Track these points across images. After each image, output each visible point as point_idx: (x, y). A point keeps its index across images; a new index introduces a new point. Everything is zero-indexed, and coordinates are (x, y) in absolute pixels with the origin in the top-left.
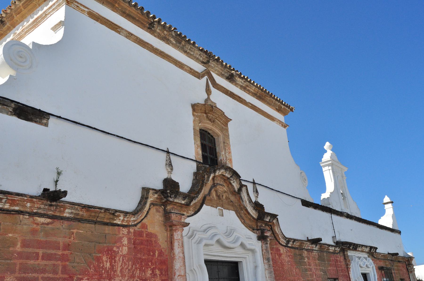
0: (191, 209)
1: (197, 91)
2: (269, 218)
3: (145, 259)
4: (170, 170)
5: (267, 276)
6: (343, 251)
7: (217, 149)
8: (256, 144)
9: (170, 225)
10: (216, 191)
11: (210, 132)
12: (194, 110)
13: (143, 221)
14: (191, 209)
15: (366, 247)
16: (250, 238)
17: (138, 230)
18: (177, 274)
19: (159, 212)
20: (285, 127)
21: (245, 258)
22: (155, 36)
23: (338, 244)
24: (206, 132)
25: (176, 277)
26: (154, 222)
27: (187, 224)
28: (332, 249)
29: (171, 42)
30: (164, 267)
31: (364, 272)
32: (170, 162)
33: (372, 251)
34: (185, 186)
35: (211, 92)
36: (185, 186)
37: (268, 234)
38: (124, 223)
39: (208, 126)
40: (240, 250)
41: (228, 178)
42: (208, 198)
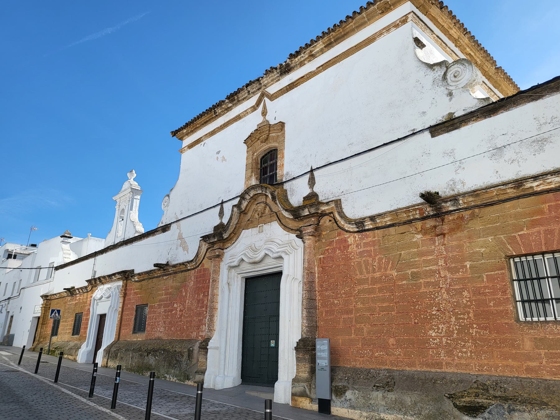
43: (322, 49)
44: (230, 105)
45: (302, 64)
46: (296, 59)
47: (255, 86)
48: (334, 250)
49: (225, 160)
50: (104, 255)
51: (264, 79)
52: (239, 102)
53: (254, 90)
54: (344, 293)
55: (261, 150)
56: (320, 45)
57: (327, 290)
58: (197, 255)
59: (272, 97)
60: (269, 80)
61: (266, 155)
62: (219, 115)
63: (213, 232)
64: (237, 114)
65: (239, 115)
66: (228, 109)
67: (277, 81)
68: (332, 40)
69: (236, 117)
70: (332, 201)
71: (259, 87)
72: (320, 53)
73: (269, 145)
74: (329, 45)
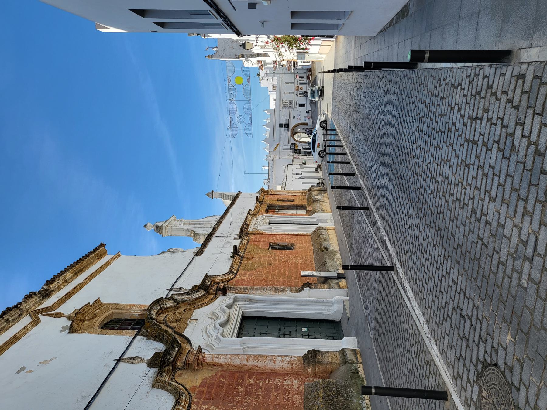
0: (184, 345)
2: (207, 281)
4: (140, 360)
6: (247, 234)
7: (126, 317)
8: (133, 280)
9: (197, 363)
10: (171, 322)
11: (106, 322)
12: (76, 331)
14: (184, 345)
15: (247, 216)
16: (222, 301)
18: (245, 362)
19: (181, 374)
20: (119, 255)
21: (240, 308)
23: (240, 236)
25: (247, 364)
26: (190, 380)
27: (200, 348)
28: (245, 242)
30: (237, 374)
31: (268, 223)
32: (130, 358)
33: (252, 214)
34: (160, 347)
35: (60, 313)
36: (160, 347)
37: (222, 285)
38: (186, 407)
39: (99, 321)
40: (232, 311)
41: (161, 309)
42: (176, 330)
45: (59, 288)
46: (53, 285)
49: (207, 195)
50: (234, 206)
56: (69, 275)
69: (12, 339)
73: (102, 317)
74: (76, 274)
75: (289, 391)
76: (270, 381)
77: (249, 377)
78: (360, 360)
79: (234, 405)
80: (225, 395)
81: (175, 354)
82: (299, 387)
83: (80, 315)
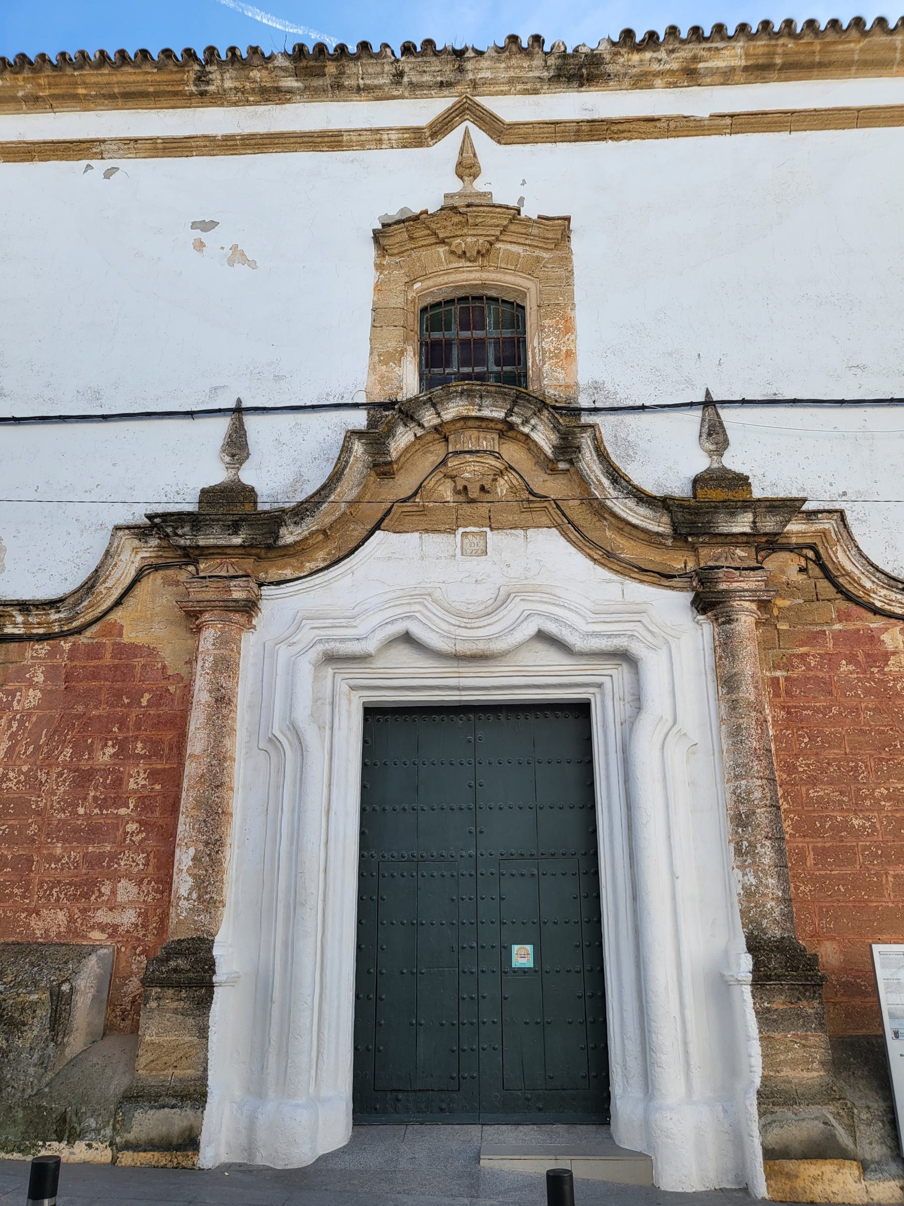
1: (479, 185)
3: (99, 717)
5: (725, 747)
13: (111, 617)
17: (90, 641)
21: (600, 686)
22: (235, 104)
24: (480, 298)
29: (290, 91)
43: (733, 69)
44: (290, 83)
45: (642, 81)
46: (636, 57)
47: (437, 70)
48: (831, 660)
51: (484, 64)
52: (338, 89)
53: (426, 78)
54: (888, 798)
55: (445, 279)
56: (733, 56)
57: (813, 781)
58: (89, 586)
59: (502, 132)
60: (504, 75)
61: (451, 302)
62: (219, 99)
63: (192, 508)
64: (334, 126)
65: (339, 133)
66: (272, 94)
67: (526, 92)
68: (778, 61)
69: (323, 134)
70: (829, 512)
71: (449, 76)
72: (717, 79)
73: (485, 275)
74: (759, 71)
75: (86, 896)
76: (137, 839)
77: (153, 775)
78: (127, 1158)
79: (38, 748)
80: (79, 717)
81: (211, 542)
82: (102, 928)
83: (457, 219)
